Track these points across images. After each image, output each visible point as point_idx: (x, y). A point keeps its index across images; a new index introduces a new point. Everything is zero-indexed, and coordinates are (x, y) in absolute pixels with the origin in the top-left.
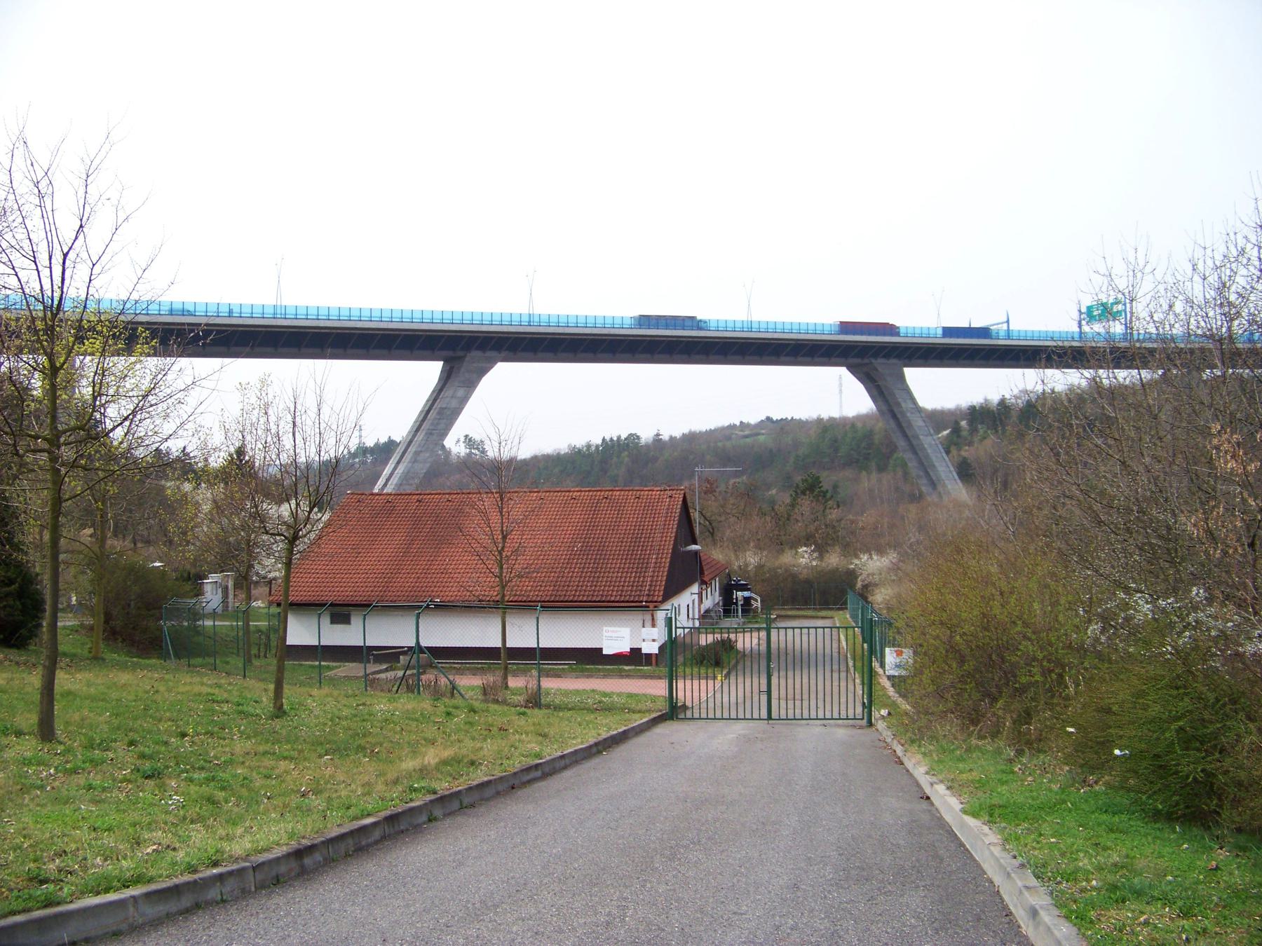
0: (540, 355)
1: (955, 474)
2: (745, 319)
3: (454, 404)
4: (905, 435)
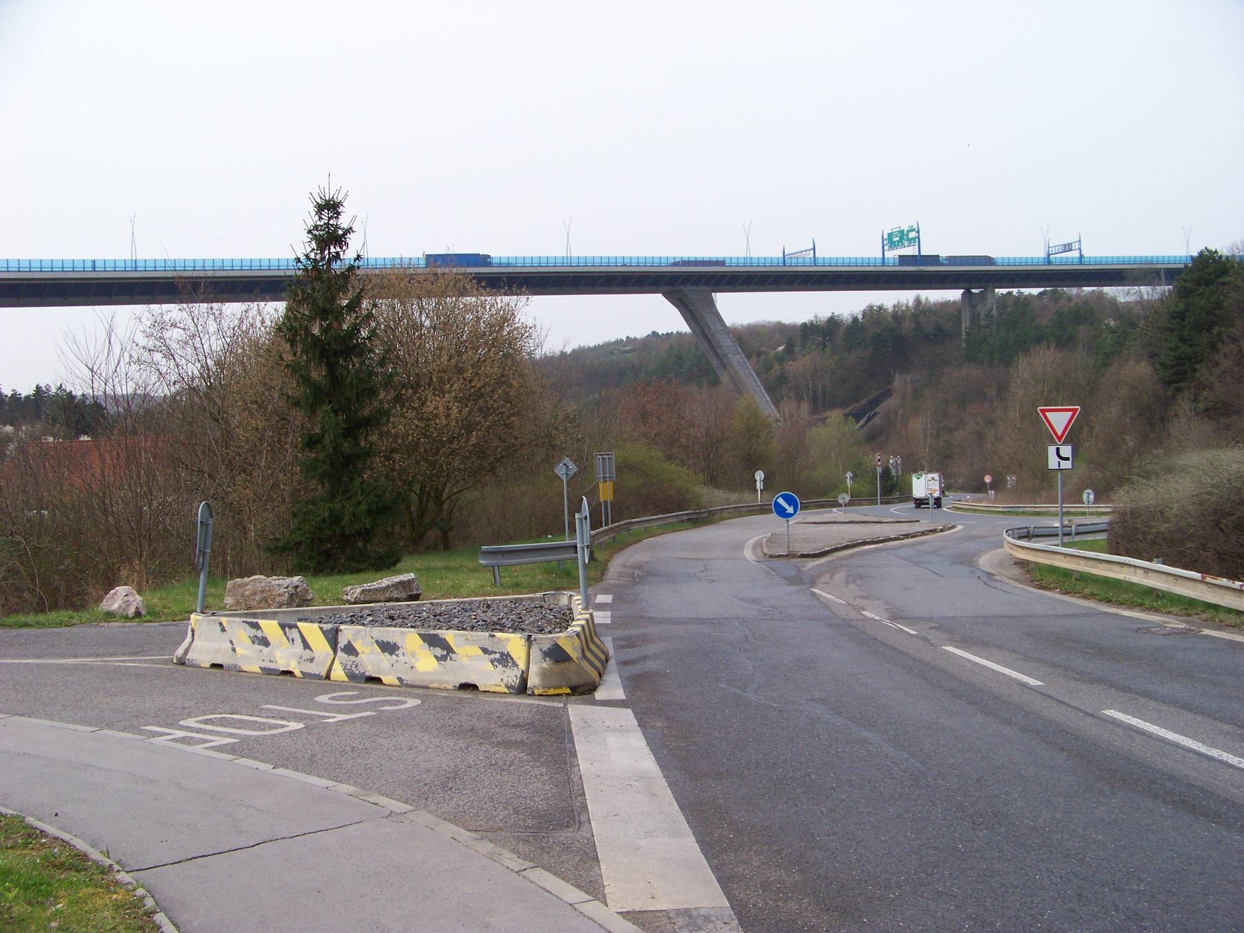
0: (597, 289)
2: (129, 257)
4: (717, 355)
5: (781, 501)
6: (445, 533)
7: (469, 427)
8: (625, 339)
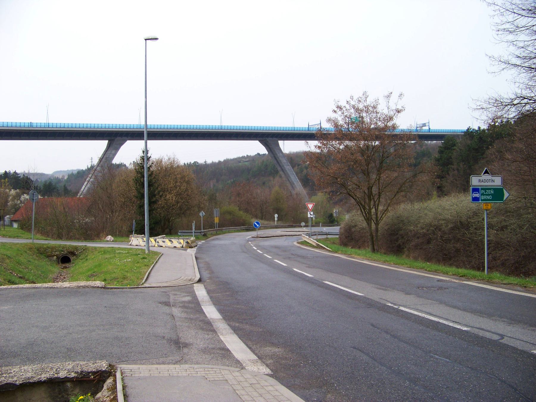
1: (298, 179)
2: (138, 124)
3: (111, 156)
4: (280, 166)
5: (256, 223)
6: (170, 230)
7: (178, 202)
8: (246, 156)
